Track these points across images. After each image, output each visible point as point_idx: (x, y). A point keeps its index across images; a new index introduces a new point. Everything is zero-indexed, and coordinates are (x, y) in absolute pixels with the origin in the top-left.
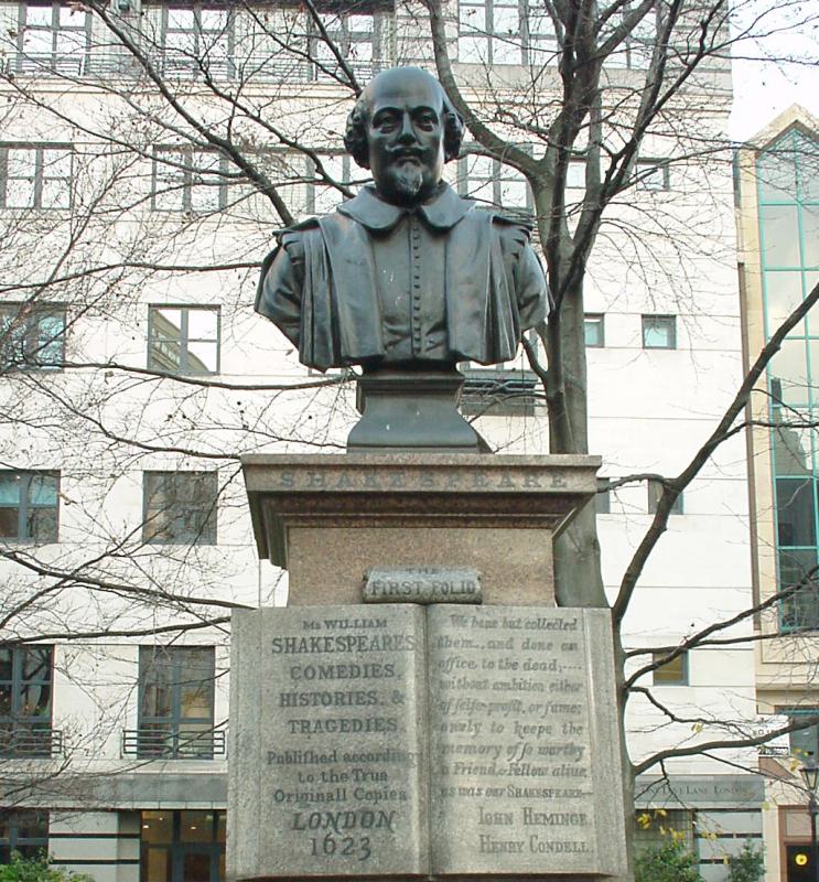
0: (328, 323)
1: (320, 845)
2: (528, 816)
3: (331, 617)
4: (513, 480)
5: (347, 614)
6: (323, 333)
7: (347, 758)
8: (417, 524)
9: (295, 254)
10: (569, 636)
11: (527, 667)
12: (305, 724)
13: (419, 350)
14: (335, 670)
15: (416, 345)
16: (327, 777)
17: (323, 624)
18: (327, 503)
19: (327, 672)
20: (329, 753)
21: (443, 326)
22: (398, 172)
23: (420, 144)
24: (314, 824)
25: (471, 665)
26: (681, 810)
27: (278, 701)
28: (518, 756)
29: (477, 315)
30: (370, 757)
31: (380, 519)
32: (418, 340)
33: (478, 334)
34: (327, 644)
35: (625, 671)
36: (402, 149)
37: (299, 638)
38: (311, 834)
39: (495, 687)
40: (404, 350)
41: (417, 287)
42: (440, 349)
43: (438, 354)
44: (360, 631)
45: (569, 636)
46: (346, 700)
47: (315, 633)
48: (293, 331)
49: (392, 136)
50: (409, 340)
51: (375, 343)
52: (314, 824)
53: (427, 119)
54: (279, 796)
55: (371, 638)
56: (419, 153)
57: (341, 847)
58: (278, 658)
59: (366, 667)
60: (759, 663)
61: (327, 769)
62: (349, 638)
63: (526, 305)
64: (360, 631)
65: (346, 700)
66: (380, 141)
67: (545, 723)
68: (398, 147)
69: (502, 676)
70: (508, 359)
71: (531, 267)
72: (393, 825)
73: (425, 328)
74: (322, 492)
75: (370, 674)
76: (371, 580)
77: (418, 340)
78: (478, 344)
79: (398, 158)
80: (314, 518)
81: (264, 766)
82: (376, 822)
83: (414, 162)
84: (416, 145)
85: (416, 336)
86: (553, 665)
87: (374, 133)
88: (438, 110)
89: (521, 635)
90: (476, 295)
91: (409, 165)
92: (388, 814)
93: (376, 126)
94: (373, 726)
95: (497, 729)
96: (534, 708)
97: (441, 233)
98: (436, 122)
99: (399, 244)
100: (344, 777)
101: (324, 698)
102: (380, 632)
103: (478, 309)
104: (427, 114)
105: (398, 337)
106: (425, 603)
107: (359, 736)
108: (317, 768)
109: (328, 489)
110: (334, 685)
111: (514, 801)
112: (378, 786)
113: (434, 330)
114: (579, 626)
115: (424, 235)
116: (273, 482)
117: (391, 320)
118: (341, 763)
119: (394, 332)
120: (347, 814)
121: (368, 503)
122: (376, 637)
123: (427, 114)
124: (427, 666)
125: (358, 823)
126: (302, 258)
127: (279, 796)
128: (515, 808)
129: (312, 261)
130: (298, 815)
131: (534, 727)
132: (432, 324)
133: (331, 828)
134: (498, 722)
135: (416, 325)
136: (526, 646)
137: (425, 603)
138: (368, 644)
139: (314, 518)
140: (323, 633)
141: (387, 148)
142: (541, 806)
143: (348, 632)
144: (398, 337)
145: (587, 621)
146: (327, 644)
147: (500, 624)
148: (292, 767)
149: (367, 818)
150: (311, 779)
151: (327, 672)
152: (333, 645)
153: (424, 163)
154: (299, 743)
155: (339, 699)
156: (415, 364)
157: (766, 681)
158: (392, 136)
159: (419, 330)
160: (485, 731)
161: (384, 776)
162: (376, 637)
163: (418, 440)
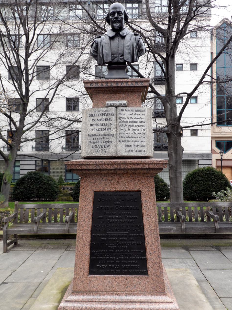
0: (102, 56)
1: (97, 150)
2: (134, 145)
3: (99, 110)
4: (133, 84)
5: (102, 109)
6: (101, 57)
7: (102, 135)
8: (116, 93)
9: (96, 43)
10: (143, 113)
11: (135, 118)
12: (95, 129)
13: (118, 60)
14: (100, 120)
15: (118, 59)
16: (98, 139)
17: (98, 111)
18: (99, 89)
19: (98, 120)
20: (98, 135)
21: (123, 55)
22: (115, 25)
23: (119, 19)
24: (96, 147)
25: (125, 118)
26: (25, 109)
27: (90, 125)
28: (133, 135)
29: (129, 53)
30: (106, 135)
31: (109, 92)
32: (118, 58)
33: (129, 57)
34: (99, 115)
35: (22, 68)
36: (115, 20)
37: (94, 114)
38: (95, 149)
39: (129, 122)
40: (115, 60)
41: (118, 48)
42: (122, 60)
43: (122, 61)
44: (105, 112)
45: (143, 113)
46: (102, 125)
47: (96, 113)
48: (154, 90)
49: (113, 17)
50: (116, 58)
51: (109, 59)
52: (96, 147)
53: (120, 14)
54: (90, 142)
55: (106, 114)
56: (118, 21)
57: (100, 151)
58: (90, 118)
59: (105, 119)
60: (212, 132)
61: (98, 137)
62: (103, 114)
63: (140, 51)
64: (105, 112)
65: (102, 125)
66: (111, 19)
67: (138, 129)
68: (115, 19)
69: (131, 120)
70: (135, 62)
71: (140, 44)
72: (110, 147)
73: (120, 56)
74: (98, 87)
75: (106, 120)
76: (107, 103)
77: (118, 58)
78: (130, 59)
79: (114, 22)
80: (97, 92)
81: (87, 137)
82: (107, 147)
83: (118, 23)
84: (118, 19)
85: (118, 57)
86: (140, 118)
87: (111, 17)
88: (123, 12)
89: (134, 113)
90: (129, 49)
91: (117, 23)
92: (109, 145)
93: (111, 16)
94: (106, 129)
95: (129, 130)
96: (136, 126)
97: (123, 37)
98: (122, 14)
99: (116, 40)
100: (101, 139)
101: (97, 124)
102: (108, 112)
103: (130, 52)
104: (120, 12)
105: (114, 58)
106: (116, 107)
107: (104, 131)
108: (96, 137)
109: (99, 86)
110: (100, 122)
111: (132, 142)
112: (107, 140)
113: (121, 56)
114: (145, 111)
115: (120, 39)
116: (89, 85)
117: (113, 54)
118: (101, 136)
119: (114, 57)
120: (102, 145)
121: (106, 89)
122: (107, 114)
123: (120, 12)
124: (117, 119)
125: (104, 146)
126: (97, 43)
127: (90, 142)
128: (132, 144)
129: (99, 44)
130: (93, 146)
131: (136, 129)
132: (121, 55)
133: (99, 148)
134: (129, 129)
135: (118, 55)
136: (135, 115)
137: (116, 107)
138: (106, 115)
139: (97, 92)
140: (98, 113)
141: (113, 20)
142: (137, 144)
143: (102, 113)
144: (114, 58)
145: (147, 110)
146: (99, 115)
147: (130, 111)
148: (92, 137)
149: (105, 146)
150: (95, 139)
151: (98, 120)
152: (100, 115)
153: (120, 22)
154: (93, 133)
155: (101, 125)
156: (118, 63)
157: (213, 136)
158: (113, 17)
159: (118, 56)
160: (127, 130)
161: (108, 138)
162: (107, 114)
163: (117, 77)
